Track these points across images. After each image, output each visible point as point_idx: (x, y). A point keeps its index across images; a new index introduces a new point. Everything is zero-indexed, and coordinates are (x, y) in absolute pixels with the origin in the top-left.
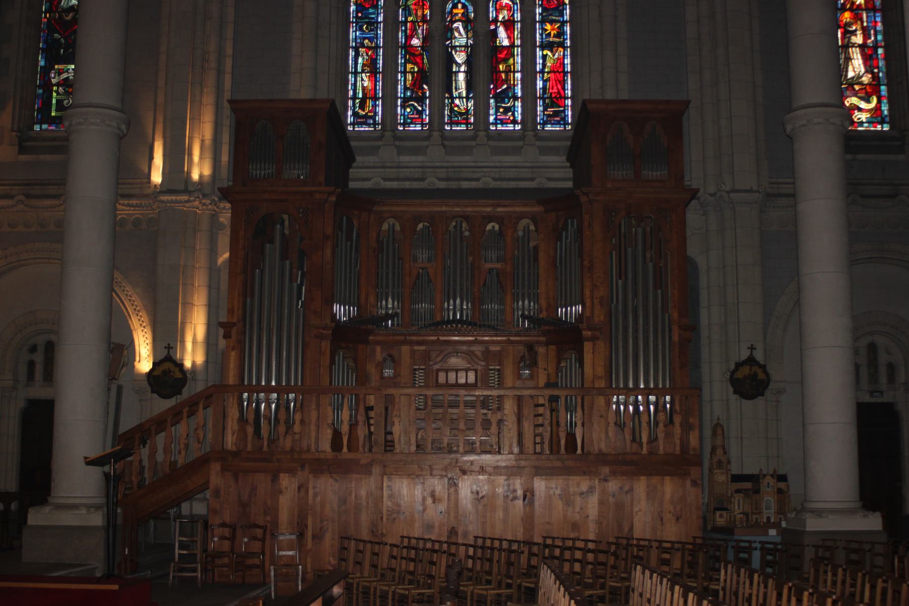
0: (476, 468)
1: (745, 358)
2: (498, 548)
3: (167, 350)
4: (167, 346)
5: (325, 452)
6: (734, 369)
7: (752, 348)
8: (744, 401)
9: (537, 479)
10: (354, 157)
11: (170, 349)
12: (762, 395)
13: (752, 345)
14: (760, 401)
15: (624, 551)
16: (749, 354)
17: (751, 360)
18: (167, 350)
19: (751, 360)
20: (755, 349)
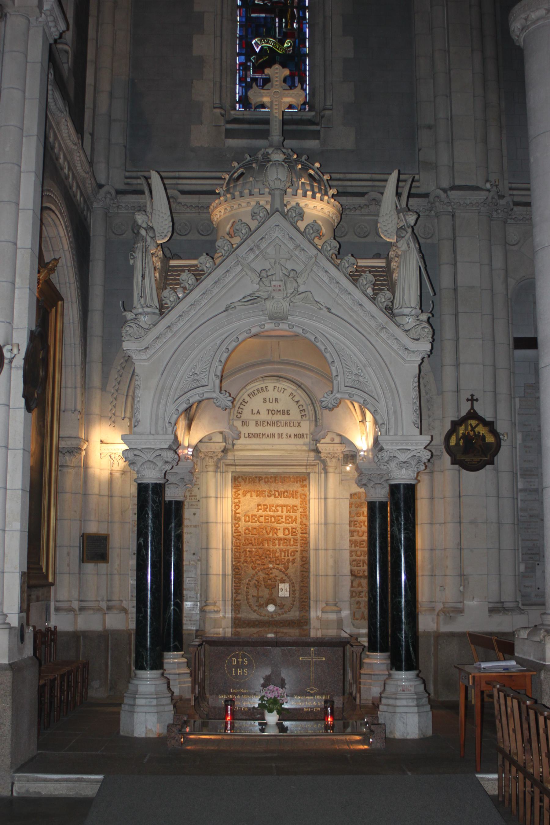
0: (507, 789)
1: (465, 414)
2: (266, 712)
3: (470, 402)
4: (470, 398)
5: (360, 668)
6: (450, 430)
7: (472, 400)
8: (464, 472)
9: (387, 664)
10: (48, 629)
11: (475, 402)
12: (492, 463)
13: (472, 396)
14: (487, 472)
15: (102, 178)
16: (469, 407)
17: (472, 415)
18: (470, 402)
19: (472, 415)
20: (477, 400)
